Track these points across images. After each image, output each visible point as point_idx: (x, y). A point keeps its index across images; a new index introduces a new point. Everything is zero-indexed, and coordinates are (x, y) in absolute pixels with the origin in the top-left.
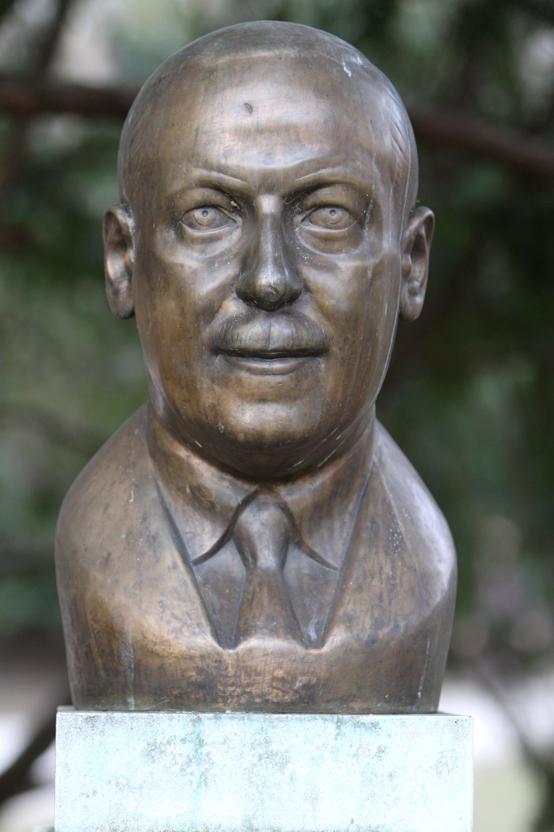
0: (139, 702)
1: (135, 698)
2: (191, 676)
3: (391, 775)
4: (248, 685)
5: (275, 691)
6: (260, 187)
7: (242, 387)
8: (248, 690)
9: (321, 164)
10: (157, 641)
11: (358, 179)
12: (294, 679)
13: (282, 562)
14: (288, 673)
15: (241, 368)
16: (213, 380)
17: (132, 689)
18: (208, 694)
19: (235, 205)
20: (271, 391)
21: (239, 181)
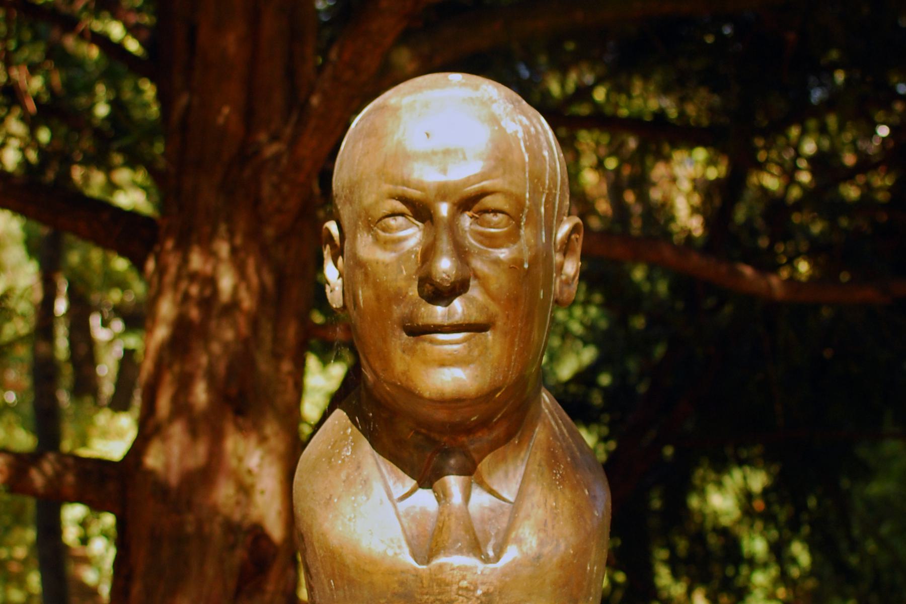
4: (439, 594)
5: (461, 598)
6: (436, 196)
8: (439, 597)
9: (483, 176)
11: (514, 189)
12: (476, 589)
13: (467, 498)
14: (471, 583)
15: (424, 340)
16: (404, 352)
20: (449, 357)
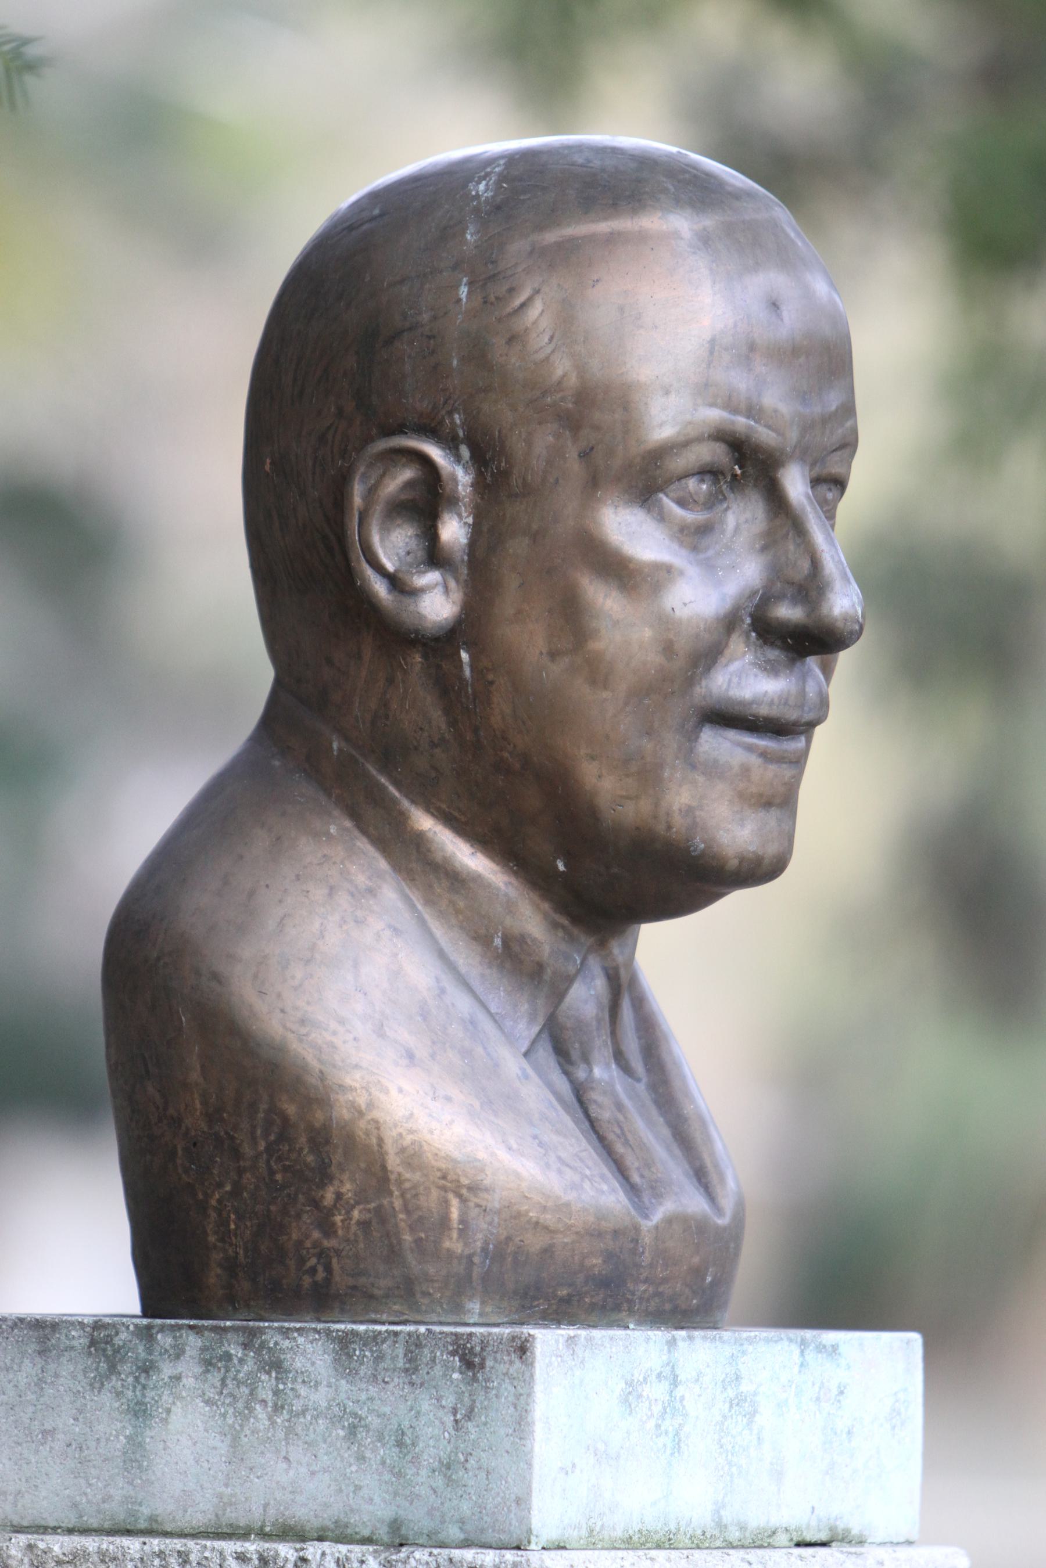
0: (489, 1309)
1: (483, 1303)
2: (594, 1266)
3: (849, 1433)
7: (749, 781)
8: (661, 1289)
10: (549, 1204)
17: (480, 1287)
18: (611, 1296)
19: (739, 472)
21: (774, 435)
